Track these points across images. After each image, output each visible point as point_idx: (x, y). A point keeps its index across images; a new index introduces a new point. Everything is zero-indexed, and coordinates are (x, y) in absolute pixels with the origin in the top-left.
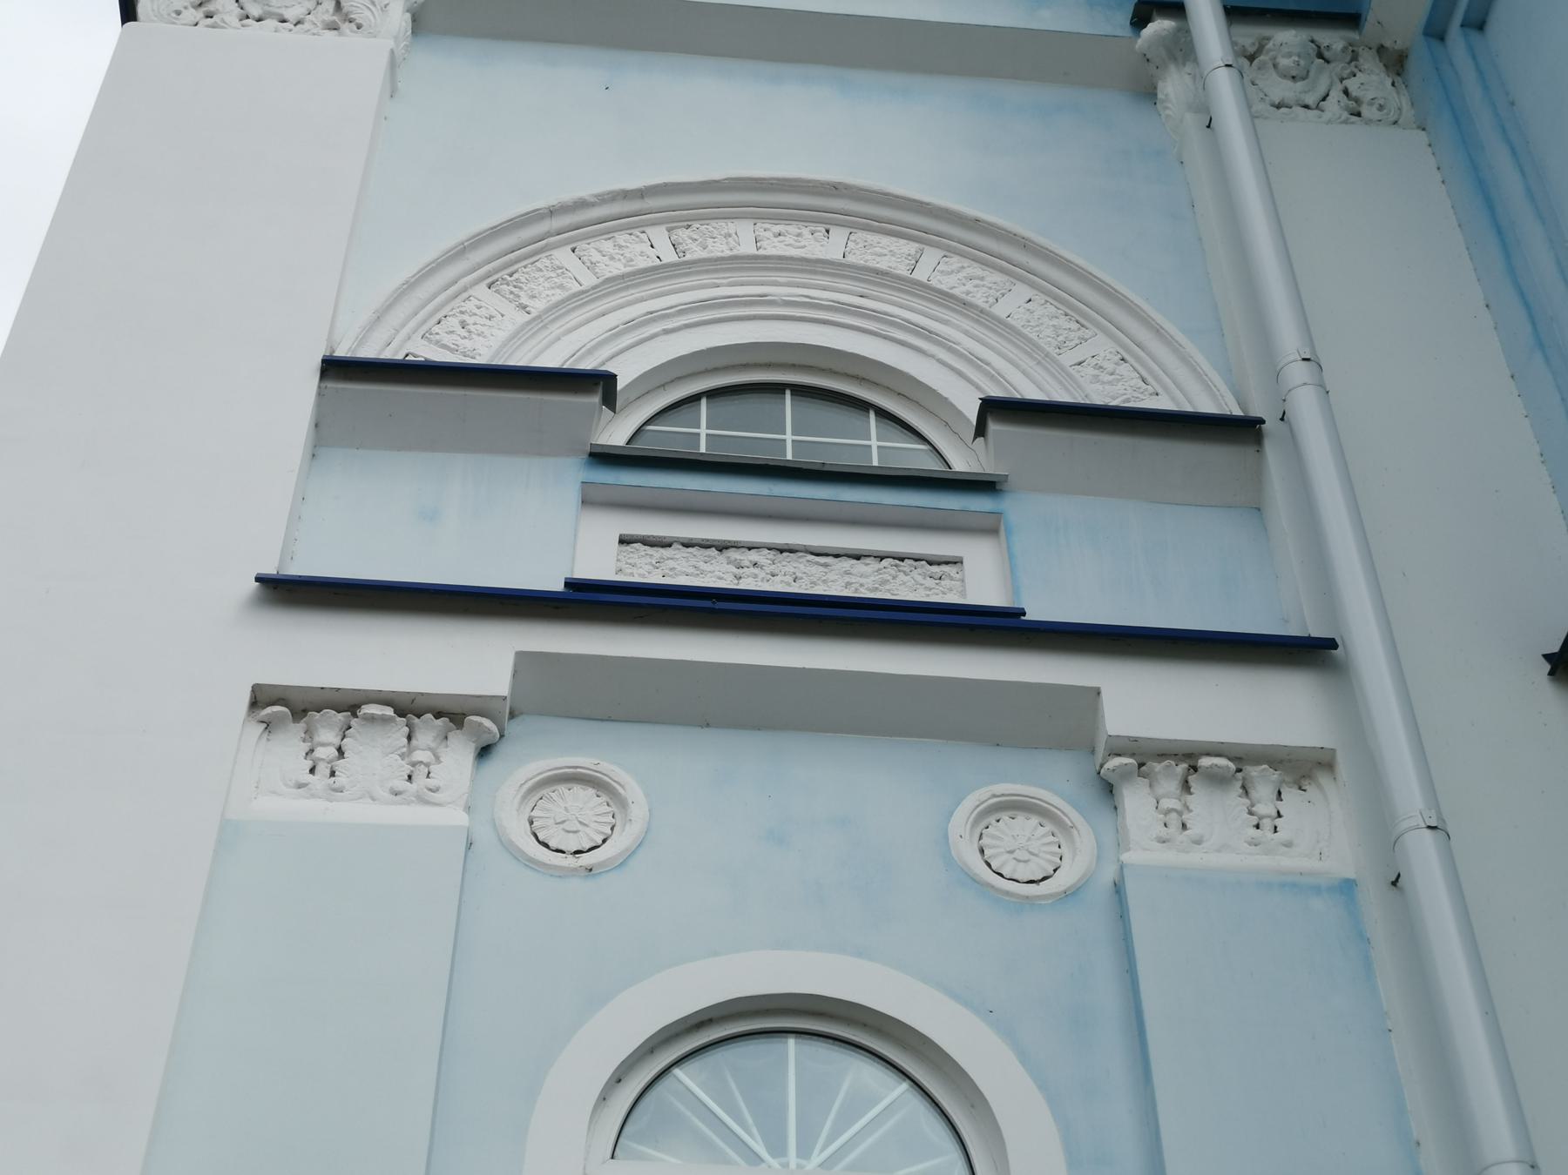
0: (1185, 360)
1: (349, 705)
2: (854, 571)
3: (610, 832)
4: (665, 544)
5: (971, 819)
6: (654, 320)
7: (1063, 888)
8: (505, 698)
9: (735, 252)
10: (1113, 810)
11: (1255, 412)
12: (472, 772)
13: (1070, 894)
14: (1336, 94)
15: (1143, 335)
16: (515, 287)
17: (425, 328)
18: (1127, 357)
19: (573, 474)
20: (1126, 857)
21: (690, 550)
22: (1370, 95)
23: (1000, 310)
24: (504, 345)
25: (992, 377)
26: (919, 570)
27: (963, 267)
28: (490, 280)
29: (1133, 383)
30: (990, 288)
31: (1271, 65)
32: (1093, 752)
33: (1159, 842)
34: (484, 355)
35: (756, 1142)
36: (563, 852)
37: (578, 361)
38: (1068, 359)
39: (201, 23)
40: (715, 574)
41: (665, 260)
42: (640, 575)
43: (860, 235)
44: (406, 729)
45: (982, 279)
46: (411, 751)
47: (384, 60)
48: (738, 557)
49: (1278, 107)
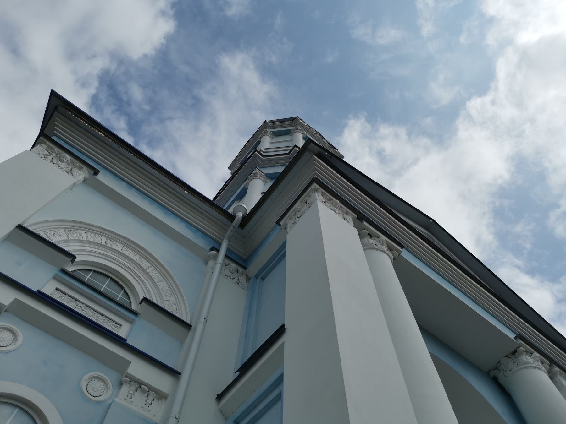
0: (186, 309)
3: (9, 345)
5: (88, 378)
7: (99, 400)
8: (6, 306)
9: (116, 249)
11: (192, 325)
13: (99, 402)
14: (236, 279)
15: (181, 301)
17: (46, 230)
18: (176, 304)
19: (55, 271)
20: (116, 399)
21: (69, 297)
22: (242, 282)
23: (158, 284)
24: (59, 241)
25: (149, 295)
26: (112, 324)
27: (157, 273)
31: (228, 268)
32: (123, 375)
33: (124, 399)
34: (54, 240)
37: (71, 251)
38: (165, 299)
39: (43, 158)
40: (71, 304)
41: (102, 243)
42: (55, 297)
45: (159, 277)
47: (73, 182)
49: (226, 276)
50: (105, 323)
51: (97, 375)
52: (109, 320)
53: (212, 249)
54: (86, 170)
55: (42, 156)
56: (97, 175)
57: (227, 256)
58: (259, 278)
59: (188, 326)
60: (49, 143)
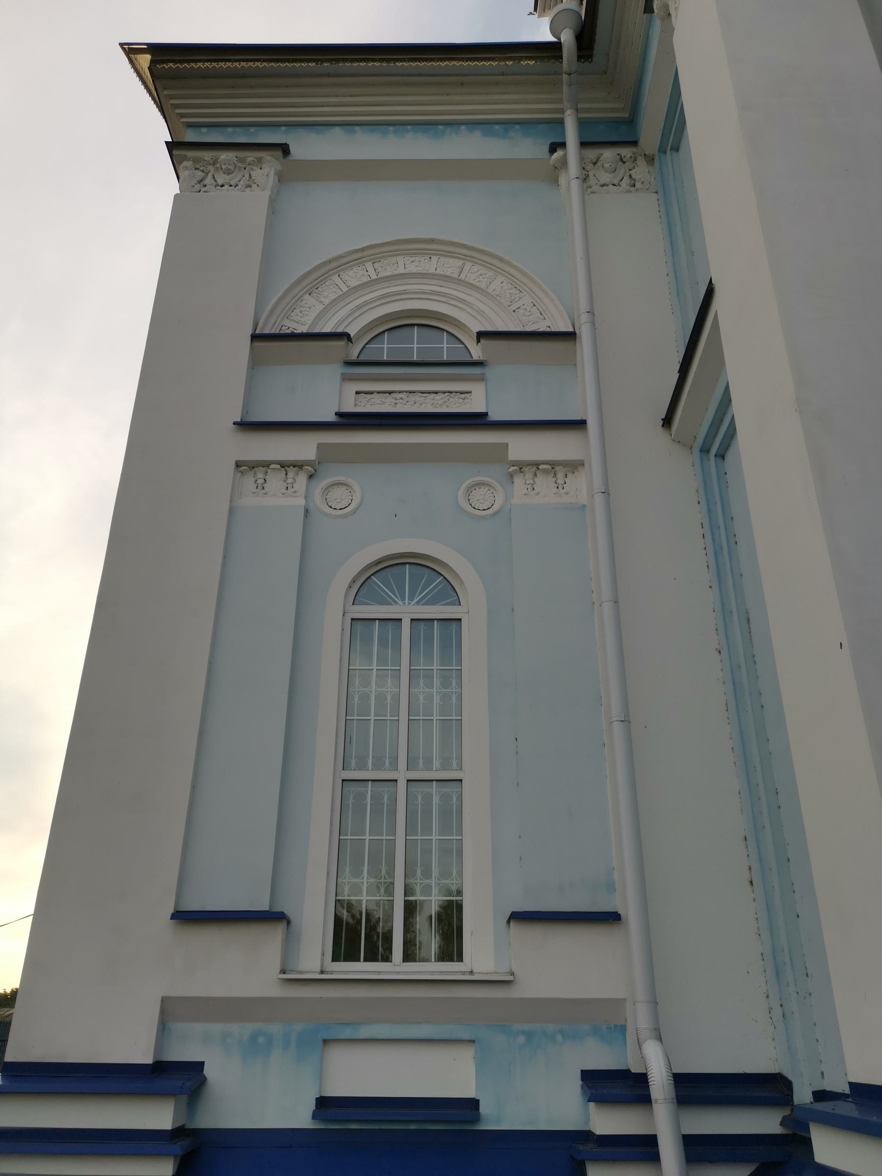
1: (266, 465)
2: (435, 398)
4: (372, 393)
6: (367, 304)
10: (512, 483)
12: (307, 483)
16: (318, 294)
19: (335, 371)
21: (380, 394)
27: (479, 270)
28: (309, 292)
29: (536, 315)
30: (488, 278)
35: (398, 598)
36: (336, 509)
43: (442, 259)
44: (285, 472)
46: (287, 479)
48: (396, 396)
50: (446, 402)
51: (474, 482)
52: (450, 394)
53: (553, 148)
54: (269, 158)
55: (198, 187)
56: (290, 151)
57: (584, 144)
58: (668, 151)
59: (570, 336)
60: (191, 154)
